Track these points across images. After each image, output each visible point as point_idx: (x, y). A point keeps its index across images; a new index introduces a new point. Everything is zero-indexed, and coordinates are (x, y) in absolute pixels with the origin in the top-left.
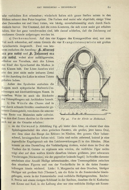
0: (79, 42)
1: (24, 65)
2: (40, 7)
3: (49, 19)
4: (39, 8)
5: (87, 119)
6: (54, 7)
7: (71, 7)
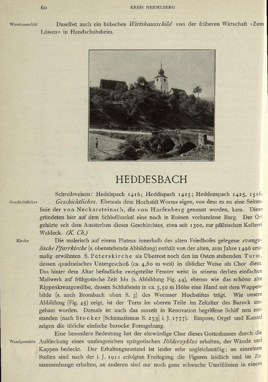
0: (101, 257)
1: (170, 202)
3: (57, 240)
4: (181, 24)
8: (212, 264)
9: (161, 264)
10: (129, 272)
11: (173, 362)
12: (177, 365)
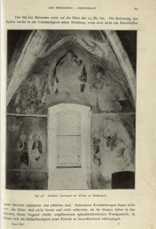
2: (53, 8)
4: (52, 8)
7: (89, 8)
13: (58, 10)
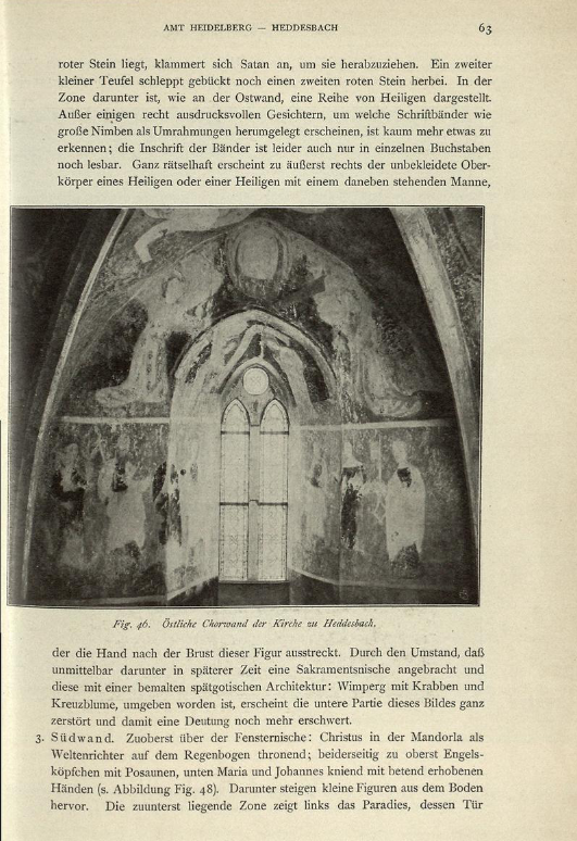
2: (179, 28)
4: (174, 28)
5: (297, 624)
6: (241, 27)
7: (313, 28)
8: (62, 756)
9: (174, 706)
10: (309, 82)
11: (105, 71)
12: (96, 64)
13: (278, 33)
